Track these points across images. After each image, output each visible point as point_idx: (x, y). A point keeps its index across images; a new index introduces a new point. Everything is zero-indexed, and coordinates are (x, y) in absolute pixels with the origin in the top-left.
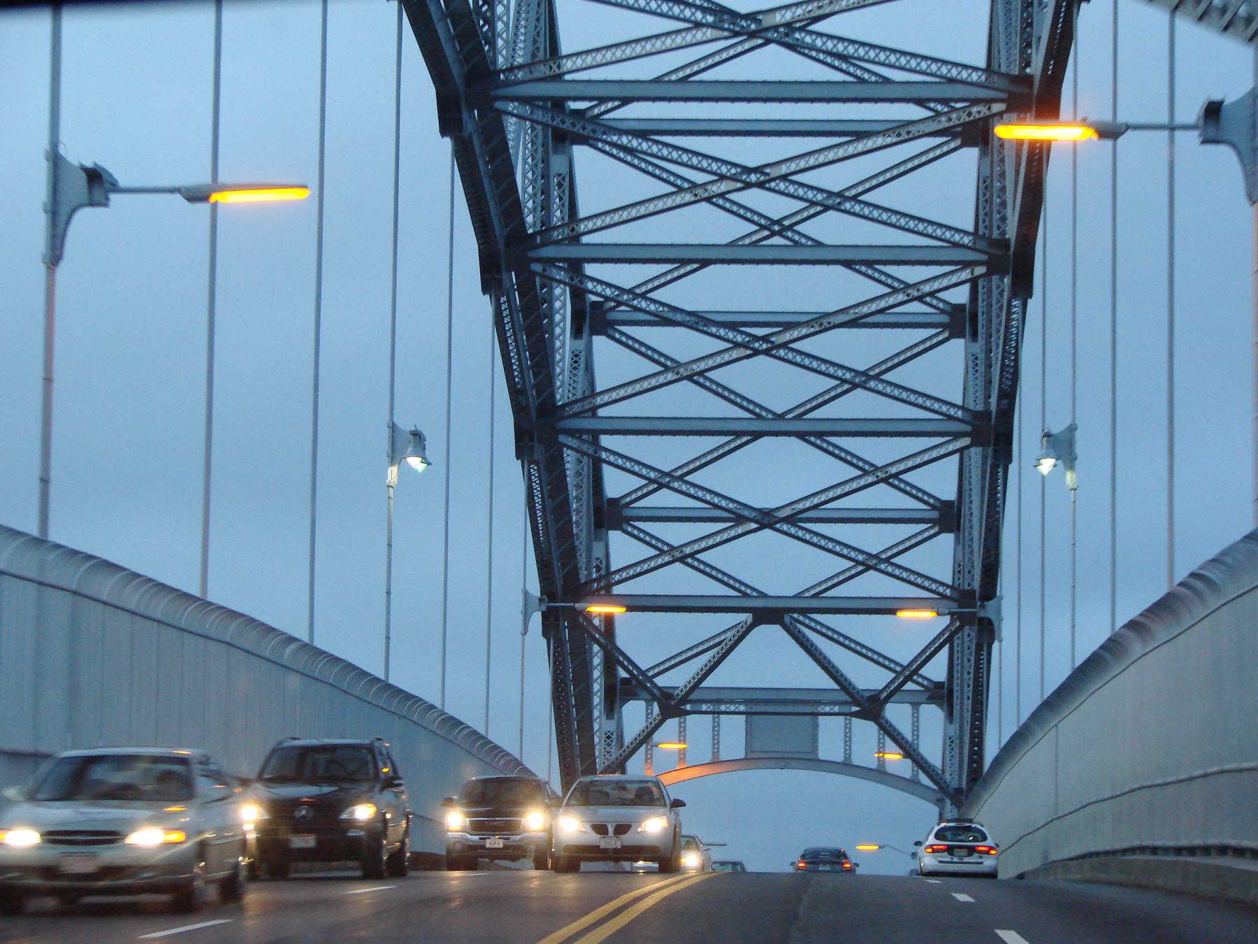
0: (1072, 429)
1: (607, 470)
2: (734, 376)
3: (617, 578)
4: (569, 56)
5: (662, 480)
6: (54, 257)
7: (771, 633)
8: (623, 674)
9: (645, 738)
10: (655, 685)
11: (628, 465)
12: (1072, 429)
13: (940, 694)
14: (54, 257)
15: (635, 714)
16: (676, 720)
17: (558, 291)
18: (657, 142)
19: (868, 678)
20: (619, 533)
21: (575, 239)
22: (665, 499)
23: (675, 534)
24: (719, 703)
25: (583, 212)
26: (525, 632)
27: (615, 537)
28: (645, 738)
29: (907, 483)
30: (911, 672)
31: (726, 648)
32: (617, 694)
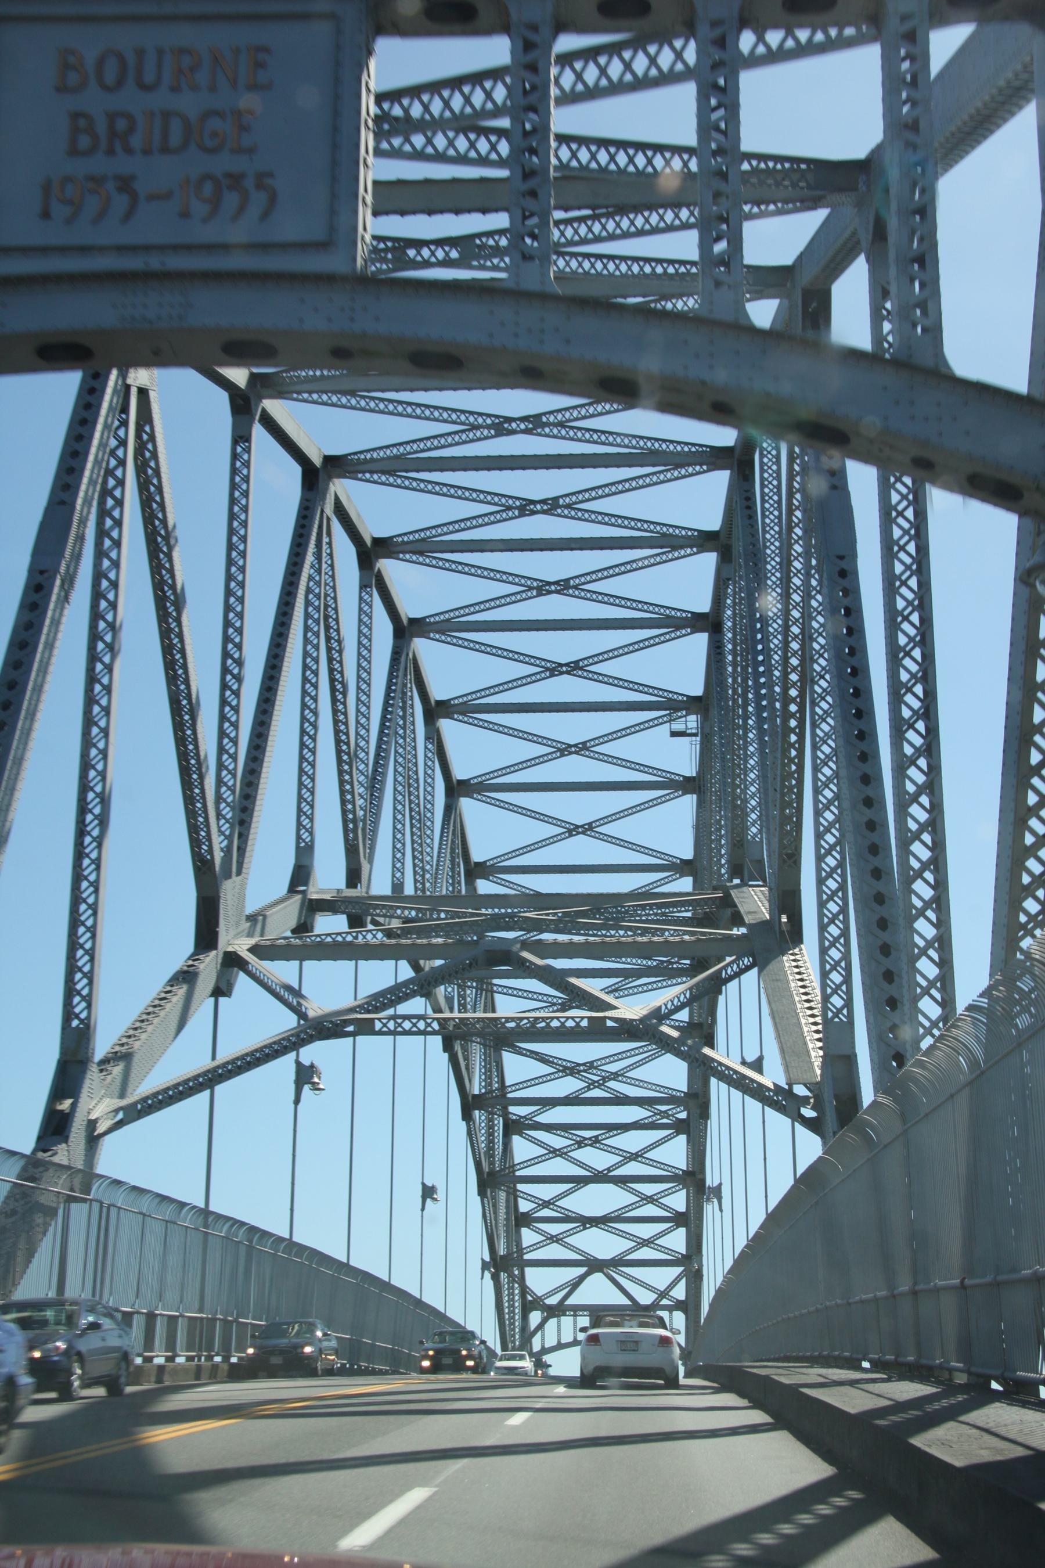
0: (720, 1185)
1: (520, 1200)
2: (579, 1154)
3: (518, 1167)
4: (509, 1086)
5: (546, 1204)
6: (423, 1209)
7: (598, 1277)
8: (530, 1298)
9: (541, 1326)
10: (544, 1303)
11: (529, 1197)
12: (720, 1185)
13: (680, 1305)
14: (423, 1209)
15: (535, 1318)
16: (556, 1319)
17: (468, 992)
18: (572, 428)
19: (645, 1298)
20: (526, 1229)
21: (504, 1095)
22: (546, 1213)
23: (554, 1229)
24: (576, 1310)
25: (508, 1083)
26: (482, 1278)
27: (524, 1231)
28: (541, 1326)
29: (662, 1204)
30: (663, 1294)
31: (575, 1285)
32: (527, 1308)
